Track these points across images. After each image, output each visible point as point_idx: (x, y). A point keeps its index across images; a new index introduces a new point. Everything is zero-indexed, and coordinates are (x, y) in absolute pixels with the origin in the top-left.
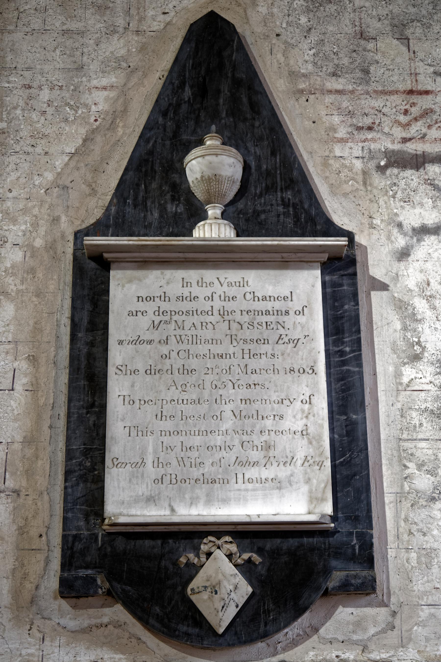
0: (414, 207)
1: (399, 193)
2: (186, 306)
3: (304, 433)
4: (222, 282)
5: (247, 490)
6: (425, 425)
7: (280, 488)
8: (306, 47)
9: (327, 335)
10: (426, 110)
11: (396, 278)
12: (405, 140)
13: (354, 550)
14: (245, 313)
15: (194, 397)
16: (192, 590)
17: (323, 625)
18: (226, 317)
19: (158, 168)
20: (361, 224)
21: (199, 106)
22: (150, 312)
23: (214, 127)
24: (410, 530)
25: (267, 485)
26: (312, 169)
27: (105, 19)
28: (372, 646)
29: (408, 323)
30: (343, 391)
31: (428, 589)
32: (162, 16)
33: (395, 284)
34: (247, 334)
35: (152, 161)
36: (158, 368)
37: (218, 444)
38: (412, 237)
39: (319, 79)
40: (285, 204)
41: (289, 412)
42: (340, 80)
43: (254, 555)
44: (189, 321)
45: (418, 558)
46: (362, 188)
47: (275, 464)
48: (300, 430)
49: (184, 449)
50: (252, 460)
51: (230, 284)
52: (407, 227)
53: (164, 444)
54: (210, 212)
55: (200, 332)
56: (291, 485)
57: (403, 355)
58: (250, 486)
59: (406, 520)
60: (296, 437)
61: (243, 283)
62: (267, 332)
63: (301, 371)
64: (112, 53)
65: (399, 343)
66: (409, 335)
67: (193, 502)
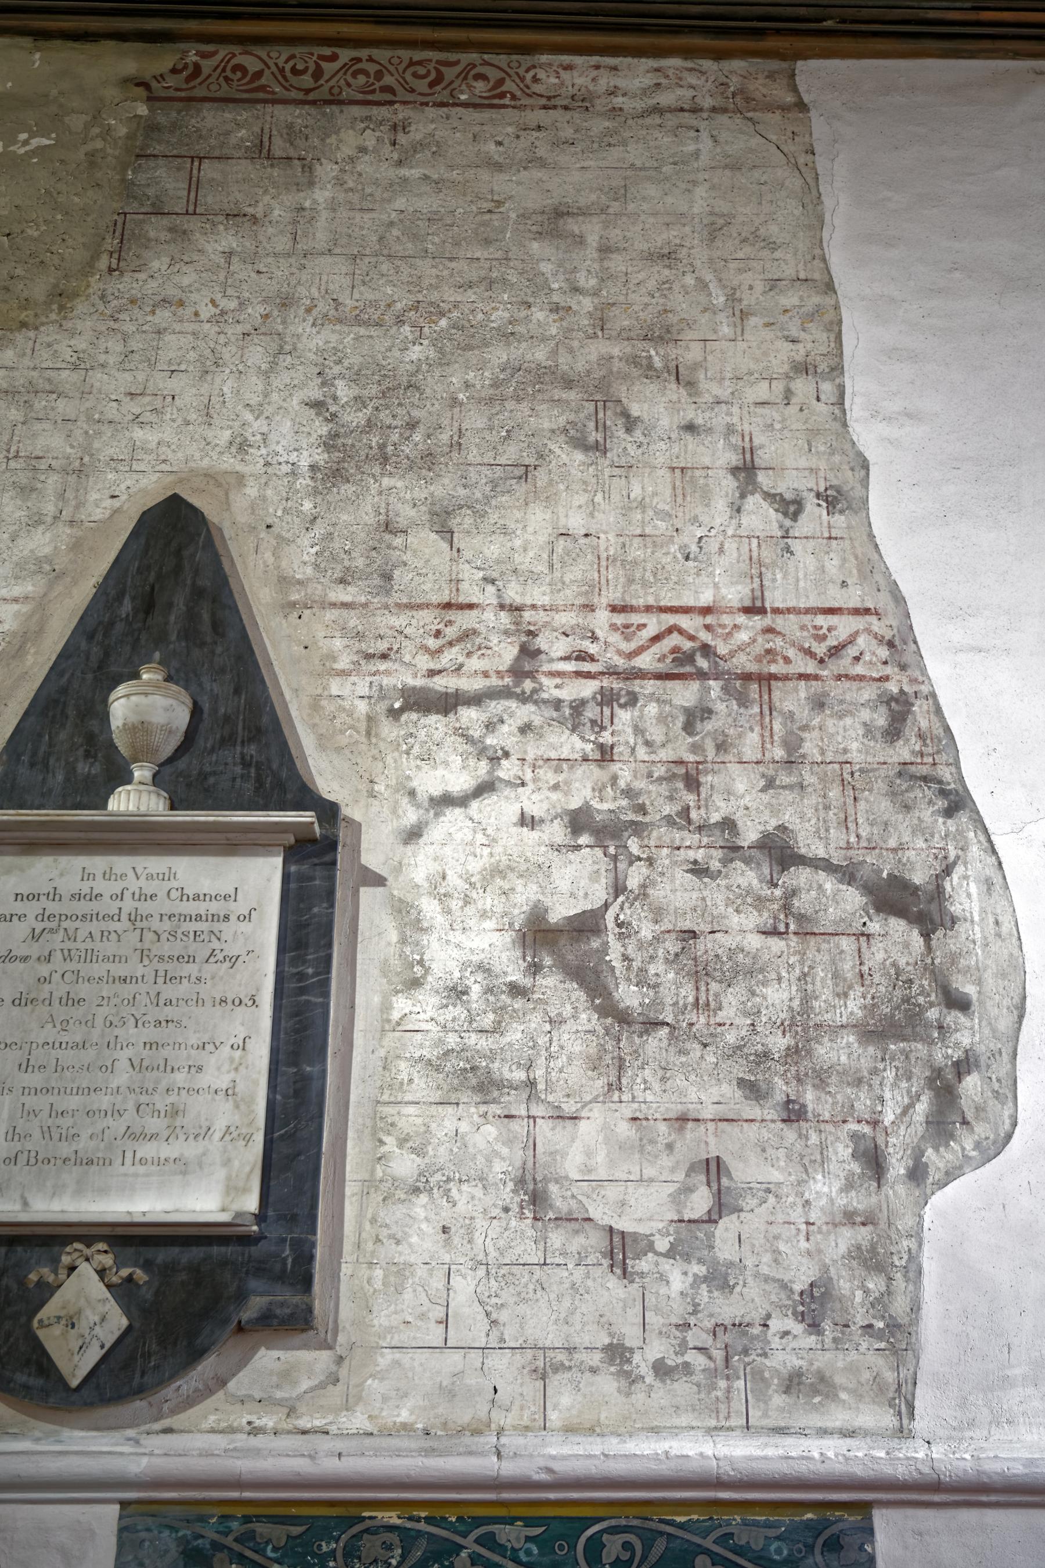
0: (435, 768)
1: (417, 748)
2: (83, 907)
3: (230, 1092)
4: (139, 873)
5: (136, 1175)
6: (416, 1081)
7: (184, 1173)
8: (306, 543)
9: (281, 950)
10: (467, 630)
11: (399, 868)
12: (432, 673)
13: (285, 1264)
14: (165, 918)
15: (78, 1038)
16: (41, 1321)
17: (234, 1375)
18: (138, 924)
19: (71, 712)
20: (357, 791)
21: (139, 625)
22: (31, 917)
23: (157, 655)
24: (377, 1236)
25: (166, 1168)
26: (294, 713)
27: (29, 504)
28: (302, 1409)
29: (408, 933)
30: (297, 1031)
31: (395, 1323)
32: (110, 501)
33: (396, 878)
34: (166, 948)
35: (65, 703)
36: (32, 996)
37: (104, 1108)
38: (427, 810)
39: (320, 587)
40: (246, 764)
41: (211, 1061)
42: (349, 588)
43: (138, 1271)
44: (84, 928)
45: (385, 1276)
46: (364, 739)
47: (182, 1137)
48: (224, 1088)
49: (54, 1114)
50: (149, 1131)
51: (150, 877)
52: (422, 796)
53: (26, 1107)
54: (137, 774)
55: (98, 945)
56: (201, 1167)
57: (395, 979)
58: (142, 1169)
59: (373, 1221)
60: (217, 1098)
61: (171, 875)
62: (195, 945)
63: (237, 1002)
64: (32, 551)
65: (392, 962)
66: (408, 950)
67: (57, 1192)
